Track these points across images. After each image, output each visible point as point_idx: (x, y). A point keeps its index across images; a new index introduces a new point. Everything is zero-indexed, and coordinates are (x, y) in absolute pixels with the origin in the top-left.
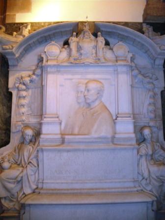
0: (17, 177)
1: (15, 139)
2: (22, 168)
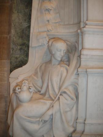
0: (43, 115)
1: (35, 56)
2: (51, 102)
